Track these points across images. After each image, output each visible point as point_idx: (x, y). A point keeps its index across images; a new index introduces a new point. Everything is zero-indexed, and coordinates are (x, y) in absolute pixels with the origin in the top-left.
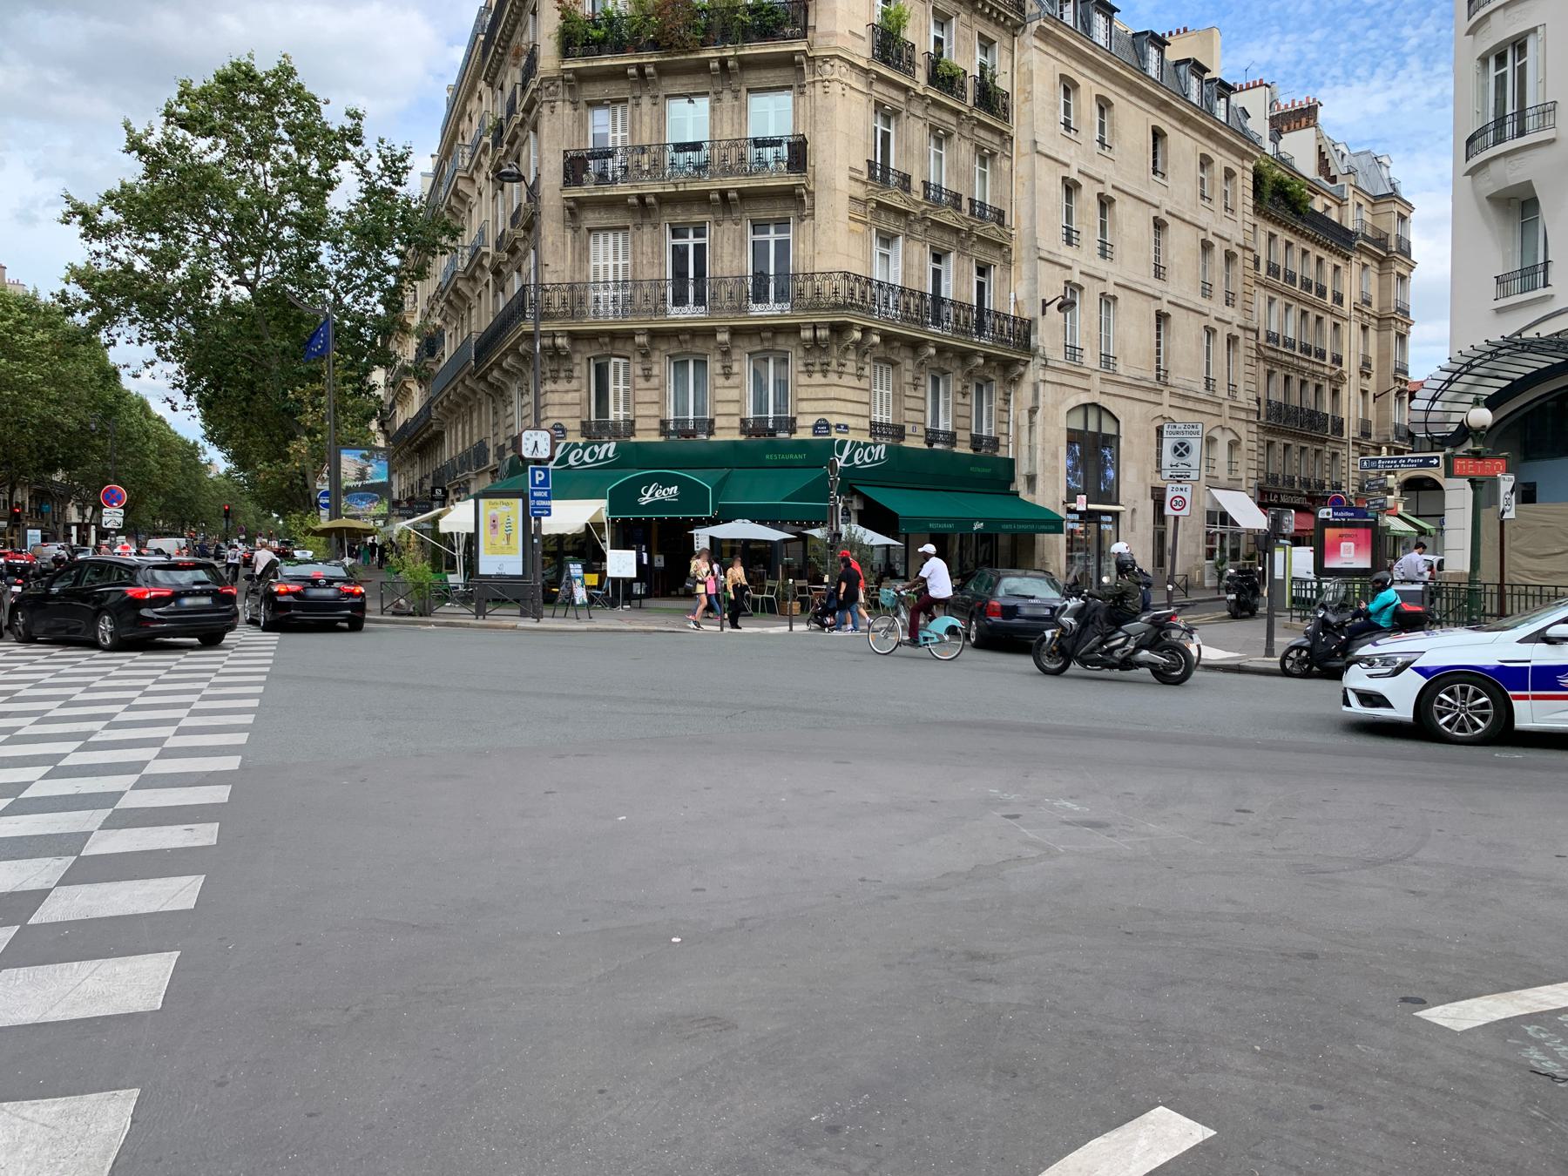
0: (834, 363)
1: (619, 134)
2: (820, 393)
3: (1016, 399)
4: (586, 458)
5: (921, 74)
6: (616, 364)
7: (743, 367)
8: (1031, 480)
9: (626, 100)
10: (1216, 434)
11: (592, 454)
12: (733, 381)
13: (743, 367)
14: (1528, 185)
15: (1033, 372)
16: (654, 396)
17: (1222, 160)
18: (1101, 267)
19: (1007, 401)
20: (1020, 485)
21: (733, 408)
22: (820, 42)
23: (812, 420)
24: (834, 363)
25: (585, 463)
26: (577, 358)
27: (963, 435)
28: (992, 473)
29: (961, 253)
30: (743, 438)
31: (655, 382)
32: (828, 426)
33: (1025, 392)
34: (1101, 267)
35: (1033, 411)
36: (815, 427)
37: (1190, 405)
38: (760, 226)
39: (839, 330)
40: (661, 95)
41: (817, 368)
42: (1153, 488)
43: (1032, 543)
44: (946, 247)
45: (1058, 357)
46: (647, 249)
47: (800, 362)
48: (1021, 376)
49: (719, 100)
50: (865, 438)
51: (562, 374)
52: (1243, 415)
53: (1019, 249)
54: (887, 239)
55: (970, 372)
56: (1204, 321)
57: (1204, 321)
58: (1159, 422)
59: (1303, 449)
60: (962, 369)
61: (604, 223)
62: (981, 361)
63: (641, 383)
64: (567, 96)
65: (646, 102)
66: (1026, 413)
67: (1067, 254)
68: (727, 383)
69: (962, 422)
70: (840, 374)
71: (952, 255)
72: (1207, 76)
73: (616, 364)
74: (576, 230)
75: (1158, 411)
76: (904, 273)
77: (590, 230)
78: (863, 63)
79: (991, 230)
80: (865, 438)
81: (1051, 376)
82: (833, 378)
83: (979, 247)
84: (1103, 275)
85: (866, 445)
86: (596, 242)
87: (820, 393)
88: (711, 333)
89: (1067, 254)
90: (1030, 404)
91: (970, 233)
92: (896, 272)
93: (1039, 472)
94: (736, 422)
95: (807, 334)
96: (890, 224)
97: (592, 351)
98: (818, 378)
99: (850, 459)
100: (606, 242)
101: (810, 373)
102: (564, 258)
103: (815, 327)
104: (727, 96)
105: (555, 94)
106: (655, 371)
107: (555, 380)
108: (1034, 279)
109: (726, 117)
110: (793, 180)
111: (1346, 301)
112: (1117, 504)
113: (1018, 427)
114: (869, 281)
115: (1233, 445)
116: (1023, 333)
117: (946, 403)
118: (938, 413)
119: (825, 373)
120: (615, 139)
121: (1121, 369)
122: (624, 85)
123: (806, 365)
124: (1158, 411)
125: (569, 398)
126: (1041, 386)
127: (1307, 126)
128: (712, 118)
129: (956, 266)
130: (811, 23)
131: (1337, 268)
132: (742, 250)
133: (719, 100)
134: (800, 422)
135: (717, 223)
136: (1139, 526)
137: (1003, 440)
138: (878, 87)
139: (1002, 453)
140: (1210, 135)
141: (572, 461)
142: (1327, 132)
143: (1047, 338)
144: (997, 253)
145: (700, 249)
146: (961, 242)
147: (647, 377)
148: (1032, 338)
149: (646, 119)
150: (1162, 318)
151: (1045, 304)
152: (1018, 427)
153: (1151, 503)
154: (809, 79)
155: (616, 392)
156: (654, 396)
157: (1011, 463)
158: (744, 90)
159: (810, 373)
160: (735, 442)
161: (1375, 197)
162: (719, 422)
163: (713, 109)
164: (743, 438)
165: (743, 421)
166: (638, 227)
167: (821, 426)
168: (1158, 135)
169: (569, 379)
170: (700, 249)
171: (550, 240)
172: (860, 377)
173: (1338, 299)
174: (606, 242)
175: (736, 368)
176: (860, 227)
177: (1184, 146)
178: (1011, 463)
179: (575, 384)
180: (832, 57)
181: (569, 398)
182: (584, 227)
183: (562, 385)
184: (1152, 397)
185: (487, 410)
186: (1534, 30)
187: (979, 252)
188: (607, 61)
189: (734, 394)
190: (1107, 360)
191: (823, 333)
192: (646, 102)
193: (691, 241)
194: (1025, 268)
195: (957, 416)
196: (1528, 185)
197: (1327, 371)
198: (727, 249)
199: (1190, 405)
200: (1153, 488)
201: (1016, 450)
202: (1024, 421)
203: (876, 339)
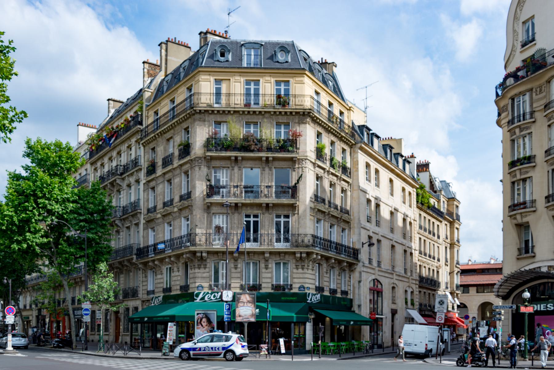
0: (306, 265)
1: (225, 179)
2: (301, 276)
3: (353, 277)
4: (212, 298)
5: (328, 163)
6: (223, 263)
7: (272, 265)
8: (359, 306)
9: (229, 167)
10: (407, 289)
11: (214, 296)
12: (268, 270)
13: (272, 265)
14: (528, 222)
15: (359, 268)
16: (239, 275)
17: (408, 188)
18: (377, 229)
19: (350, 278)
20: (355, 308)
21: (269, 280)
22: (301, 154)
23: (298, 286)
24: (306, 265)
25: (211, 300)
26: (208, 260)
27: (339, 290)
28: (346, 305)
29: (338, 225)
30: (272, 291)
31: (239, 270)
32: (304, 288)
33: (356, 275)
34: (377, 229)
35: (360, 282)
36: (299, 288)
37: (400, 278)
38: (278, 216)
39: (309, 254)
40: (242, 166)
41: (300, 267)
42: (392, 309)
43: (360, 330)
44: (334, 223)
45: (367, 262)
46: (236, 222)
47: (294, 265)
48: (355, 269)
49: (264, 170)
50: (314, 292)
51: (202, 266)
52: (414, 282)
53: (354, 224)
54: (318, 221)
55: (149, 222)
56: (391, 242)
57: (391, 242)
58: (392, 285)
59: (425, 292)
60: (327, 263)
61: (219, 211)
62: (333, 261)
63: (233, 270)
64: (206, 164)
65: (236, 169)
66: (357, 282)
67: (368, 225)
68: (267, 271)
69: (339, 286)
70: (308, 269)
71: (336, 226)
72: (371, 132)
73: (223, 263)
74: (208, 213)
75: (392, 281)
76: (324, 233)
77: (213, 213)
78: (313, 161)
79: (345, 216)
80: (314, 292)
81: (365, 269)
82: (306, 271)
83: (343, 223)
84: (368, 229)
85: (315, 294)
86: (215, 218)
87: (301, 276)
88: (263, 253)
89: (368, 225)
90: (358, 279)
91: (341, 219)
92: (321, 233)
93: (362, 303)
94: (270, 285)
95: (298, 255)
96: (320, 216)
97: (215, 258)
98: (300, 270)
99: (311, 300)
100: (219, 218)
101: (297, 269)
102: (203, 223)
103: (301, 253)
104: (267, 169)
105: (201, 163)
106: (239, 266)
107: (199, 268)
108: (360, 234)
109: (267, 176)
110: (292, 201)
111: (441, 238)
112: (382, 315)
113: (354, 287)
114: (331, 242)
115: (412, 292)
116: (355, 253)
117: (334, 279)
118: (333, 282)
119: (303, 269)
120: (223, 181)
121: (382, 266)
122: (229, 162)
123: (296, 266)
124: (392, 281)
125: (205, 275)
126: (362, 273)
127: (426, 171)
128: (359, 216)
129: (337, 230)
130: (298, 147)
131: (438, 226)
132: (272, 224)
133: (264, 170)
134: (294, 286)
135: (263, 214)
136: (388, 323)
137: (349, 292)
138: (317, 169)
139: (349, 297)
140: (404, 180)
141: (206, 299)
142: (434, 174)
143: (363, 256)
144: (347, 225)
145: (256, 223)
146: (338, 221)
147: (236, 268)
148: (359, 255)
149: (236, 175)
150: (393, 246)
151: (363, 244)
152: (354, 287)
153: (390, 315)
154: (297, 166)
155: (223, 274)
156: (239, 275)
157: (351, 300)
158: (273, 167)
159: (297, 269)
160: (270, 293)
161: (448, 199)
162: (263, 285)
163: (262, 174)
164: (272, 291)
165: (272, 285)
166: (233, 214)
167: (302, 287)
168: (391, 181)
169: (205, 268)
170: (256, 223)
171: (198, 216)
172: (313, 270)
173: (439, 237)
174: (219, 218)
175: (270, 266)
176: (312, 218)
177: (398, 184)
178: (351, 300)
179: (207, 270)
180: (306, 159)
181: (205, 275)
182: (212, 212)
183: (202, 270)
184: (390, 276)
185: (140, 274)
186: (529, 177)
187: (343, 225)
188: (224, 154)
189: (269, 275)
190: (379, 263)
191: (304, 255)
192: (236, 169)
193: (252, 219)
194: (356, 231)
195: (337, 283)
196: (528, 222)
197: (436, 264)
198: (267, 223)
199: (400, 278)
200: (392, 309)
201: (354, 296)
202: (356, 285)
203: (319, 257)
